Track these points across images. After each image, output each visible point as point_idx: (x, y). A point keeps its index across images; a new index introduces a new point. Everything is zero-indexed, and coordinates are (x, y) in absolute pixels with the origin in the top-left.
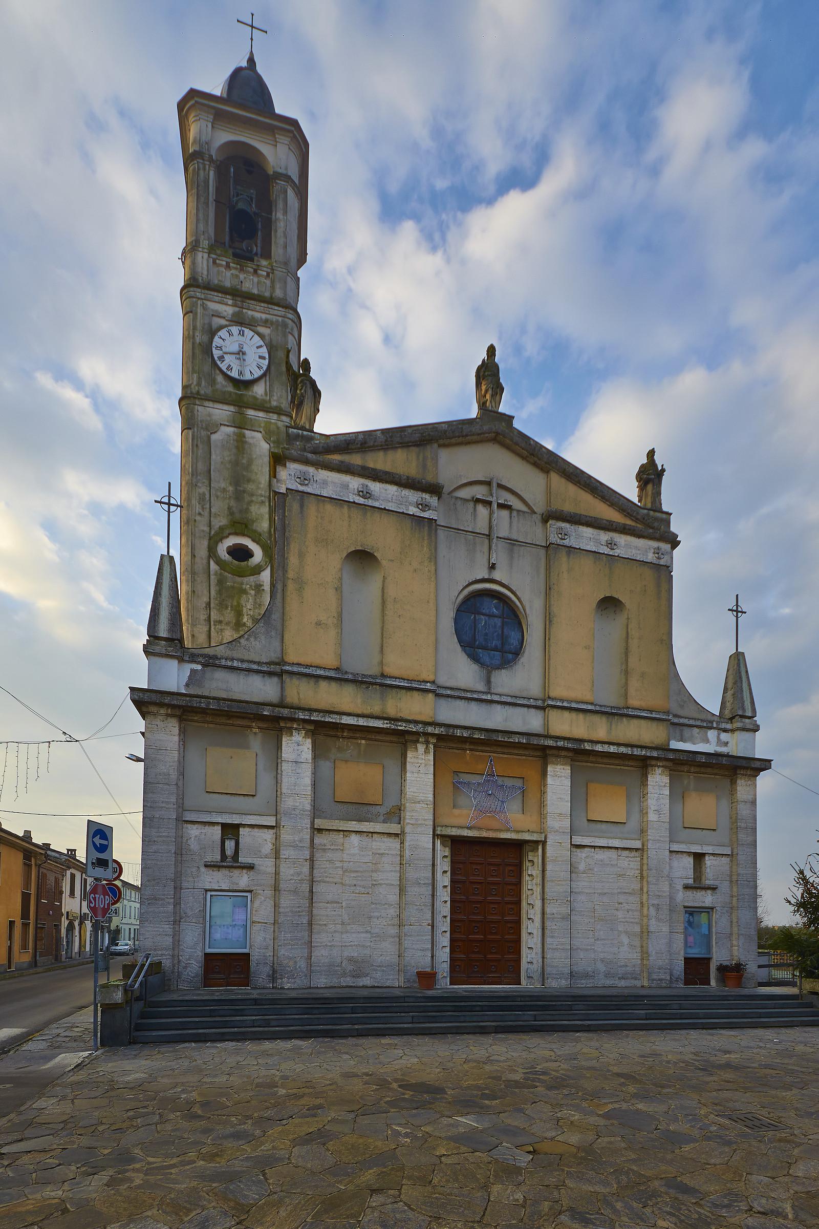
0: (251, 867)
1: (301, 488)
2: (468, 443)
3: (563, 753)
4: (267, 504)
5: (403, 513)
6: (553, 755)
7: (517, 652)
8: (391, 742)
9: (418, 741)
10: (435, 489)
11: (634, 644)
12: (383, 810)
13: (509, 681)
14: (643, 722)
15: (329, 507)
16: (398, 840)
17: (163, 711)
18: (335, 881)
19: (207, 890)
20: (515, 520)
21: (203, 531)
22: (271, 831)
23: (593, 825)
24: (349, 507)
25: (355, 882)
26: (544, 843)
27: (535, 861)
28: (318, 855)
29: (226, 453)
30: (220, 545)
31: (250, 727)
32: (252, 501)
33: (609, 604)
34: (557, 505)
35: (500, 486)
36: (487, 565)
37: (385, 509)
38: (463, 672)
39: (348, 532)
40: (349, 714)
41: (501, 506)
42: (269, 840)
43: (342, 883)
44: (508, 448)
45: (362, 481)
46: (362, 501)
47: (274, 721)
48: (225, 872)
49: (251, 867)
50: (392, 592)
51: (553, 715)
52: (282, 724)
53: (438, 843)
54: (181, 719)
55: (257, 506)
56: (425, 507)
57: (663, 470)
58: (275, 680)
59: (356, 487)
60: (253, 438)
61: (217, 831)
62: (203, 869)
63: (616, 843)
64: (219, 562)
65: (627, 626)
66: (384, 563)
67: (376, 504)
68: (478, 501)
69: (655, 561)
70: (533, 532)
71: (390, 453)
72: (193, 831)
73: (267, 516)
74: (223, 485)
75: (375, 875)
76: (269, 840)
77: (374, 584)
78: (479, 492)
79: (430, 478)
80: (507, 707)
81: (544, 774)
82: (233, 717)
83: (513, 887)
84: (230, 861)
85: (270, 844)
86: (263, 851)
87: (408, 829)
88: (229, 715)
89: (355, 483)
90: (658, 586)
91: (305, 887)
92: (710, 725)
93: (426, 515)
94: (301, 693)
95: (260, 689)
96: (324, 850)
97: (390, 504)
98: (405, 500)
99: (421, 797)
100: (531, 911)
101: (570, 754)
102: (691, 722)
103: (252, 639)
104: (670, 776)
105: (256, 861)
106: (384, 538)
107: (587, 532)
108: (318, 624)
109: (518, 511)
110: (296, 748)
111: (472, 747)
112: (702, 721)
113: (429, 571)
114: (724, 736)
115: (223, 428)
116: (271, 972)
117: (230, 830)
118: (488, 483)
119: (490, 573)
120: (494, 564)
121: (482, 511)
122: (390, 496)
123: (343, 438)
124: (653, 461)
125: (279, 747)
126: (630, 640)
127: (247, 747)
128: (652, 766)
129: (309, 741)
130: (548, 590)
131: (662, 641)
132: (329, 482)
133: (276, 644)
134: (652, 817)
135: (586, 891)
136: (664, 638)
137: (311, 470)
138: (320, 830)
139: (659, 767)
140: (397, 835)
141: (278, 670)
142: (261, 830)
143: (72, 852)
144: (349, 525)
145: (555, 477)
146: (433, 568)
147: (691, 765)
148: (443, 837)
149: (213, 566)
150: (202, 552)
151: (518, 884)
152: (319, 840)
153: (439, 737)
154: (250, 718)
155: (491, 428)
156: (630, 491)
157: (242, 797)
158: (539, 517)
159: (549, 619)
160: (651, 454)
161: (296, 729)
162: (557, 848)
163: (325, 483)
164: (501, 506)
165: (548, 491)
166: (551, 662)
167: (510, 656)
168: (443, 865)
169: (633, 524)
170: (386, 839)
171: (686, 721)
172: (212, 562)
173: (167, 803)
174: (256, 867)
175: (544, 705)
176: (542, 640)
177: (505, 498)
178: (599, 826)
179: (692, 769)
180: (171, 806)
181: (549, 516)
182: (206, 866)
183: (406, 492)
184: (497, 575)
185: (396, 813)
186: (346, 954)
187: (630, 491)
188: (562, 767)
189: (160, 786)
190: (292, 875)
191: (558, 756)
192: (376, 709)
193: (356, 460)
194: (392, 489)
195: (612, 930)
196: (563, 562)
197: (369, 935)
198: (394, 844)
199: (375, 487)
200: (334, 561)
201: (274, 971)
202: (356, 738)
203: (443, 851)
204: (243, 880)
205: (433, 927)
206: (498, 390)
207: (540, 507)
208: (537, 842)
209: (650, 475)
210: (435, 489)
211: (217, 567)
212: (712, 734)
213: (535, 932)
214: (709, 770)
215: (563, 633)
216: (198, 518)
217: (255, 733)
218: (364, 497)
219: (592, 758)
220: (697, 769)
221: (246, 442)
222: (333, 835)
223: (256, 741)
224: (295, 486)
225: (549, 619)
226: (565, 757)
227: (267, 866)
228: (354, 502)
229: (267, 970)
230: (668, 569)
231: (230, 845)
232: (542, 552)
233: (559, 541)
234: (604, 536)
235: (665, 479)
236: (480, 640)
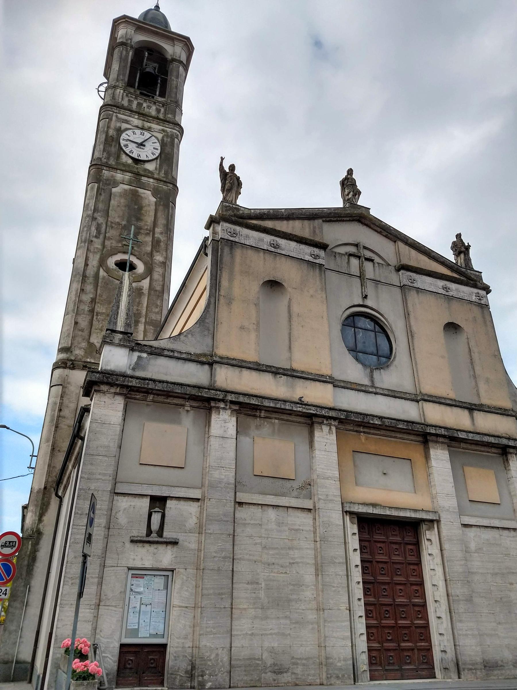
0: (175, 543)
1: (232, 239)
2: (343, 221)
3: (441, 440)
4: (151, 235)
5: (301, 259)
6: (433, 441)
7: (389, 355)
8: (299, 423)
9: (322, 423)
10: (323, 247)
11: (476, 356)
12: (295, 485)
13: (387, 379)
15: (250, 252)
16: (310, 516)
17: (113, 390)
18: (255, 558)
19: (129, 569)
20: (377, 269)
21: (97, 248)
22: (196, 504)
23: (475, 505)
24: (264, 253)
25: (273, 561)
26: (438, 521)
27: (433, 539)
28: (238, 530)
29: (122, 200)
30: (110, 259)
31: (183, 406)
32: (140, 232)
33: (452, 327)
34: (405, 261)
35: (365, 248)
36: (361, 295)
37: (289, 256)
38: (354, 371)
39: (265, 267)
41: (367, 259)
42: (194, 514)
43: (261, 561)
44: (367, 225)
45: (273, 238)
46: (273, 249)
47: (204, 401)
48: (152, 548)
49: (175, 543)
50: (295, 309)
51: (477, 415)
52: (213, 404)
53: (347, 518)
54: (126, 397)
55: (143, 236)
56: (317, 257)
57: (469, 246)
58: (207, 367)
59: (269, 241)
60: (144, 193)
61: (146, 502)
62: (128, 545)
64: (107, 270)
65: (468, 344)
66: (290, 289)
67: (283, 252)
68: (351, 255)
69: (477, 301)
70: (394, 278)
71: (291, 222)
72: (123, 503)
73: (150, 243)
74: (117, 220)
75: (291, 552)
76: (194, 514)
77: (282, 304)
78: (352, 250)
79: (317, 239)
81: (427, 457)
82: (171, 396)
83: (415, 567)
84: (154, 536)
85: (194, 518)
86: (187, 525)
87: (320, 505)
88: (168, 394)
89: (268, 238)
90: (484, 317)
91: (228, 565)
93: (317, 261)
94: (226, 378)
95: (193, 375)
96: (245, 525)
97: (292, 253)
98: (302, 251)
99: (329, 473)
100: (437, 594)
101: (446, 441)
103: (190, 336)
104: (449, 451)
105: (181, 537)
106: (288, 273)
107: (429, 280)
108: (242, 328)
109: (378, 263)
110: (223, 425)
111: (366, 430)
113: (322, 297)
115: (121, 185)
116: (189, 668)
117: (158, 502)
118: (357, 245)
119: (363, 302)
120: (366, 296)
121: (355, 262)
122: (292, 248)
123: (258, 211)
124: (462, 240)
125: (208, 423)
126: (472, 354)
127: (177, 421)
128: (511, 453)
129: (234, 419)
130: (407, 315)
131: (495, 356)
132: (252, 237)
133: (209, 341)
135: (480, 571)
136: (496, 354)
137: (238, 228)
138: (240, 504)
140: (309, 510)
141: (210, 361)
142: (486, 529)
144: (264, 264)
145: (401, 245)
146: (324, 296)
148: (351, 513)
149: (102, 273)
150: (94, 261)
151: (419, 563)
152: (242, 513)
153: (341, 421)
154: (185, 398)
155: (354, 214)
156: (450, 256)
158: (393, 268)
159: (410, 334)
160: (459, 236)
161: (224, 408)
162: (450, 526)
163: (247, 236)
164: (367, 259)
165: (398, 254)
166: (419, 366)
167: (384, 360)
168: (354, 543)
169: (458, 277)
170: (299, 513)
172: (101, 270)
173: (105, 475)
174: (180, 542)
175: (418, 398)
176: (409, 350)
177: (368, 254)
180: (107, 478)
181: (403, 268)
182: (132, 541)
183: (303, 246)
184: (369, 303)
185: (307, 487)
186: (266, 644)
187: (450, 256)
188: (441, 451)
189: (100, 458)
190: (215, 552)
191: (437, 442)
193: (269, 224)
194: (293, 244)
195: (509, 612)
196: (412, 297)
197: (288, 622)
198: (303, 520)
199: (282, 242)
200: (255, 287)
201: (193, 667)
202: (270, 418)
203: (353, 528)
204: (166, 557)
205: (350, 611)
206: (357, 193)
207: (393, 261)
208: (432, 521)
209: (461, 248)
210: (323, 247)
211: (105, 274)
213: (443, 616)
215: (422, 345)
216: (94, 239)
217: (188, 411)
218: (275, 247)
219: (462, 445)
221: (139, 196)
222: (253, 509)
223: (300, 434)
224: (227, 237)
225: (410, 334)
226: (442, 443)
227: (189, 541)
228: (268, 250)
229: (184, 665)
230: (487, 306)
231: (156, 518)
232: (398, 290)
233: (410, 284)
234: (441, 283)
235: (471, 251)
236: (360, 346)
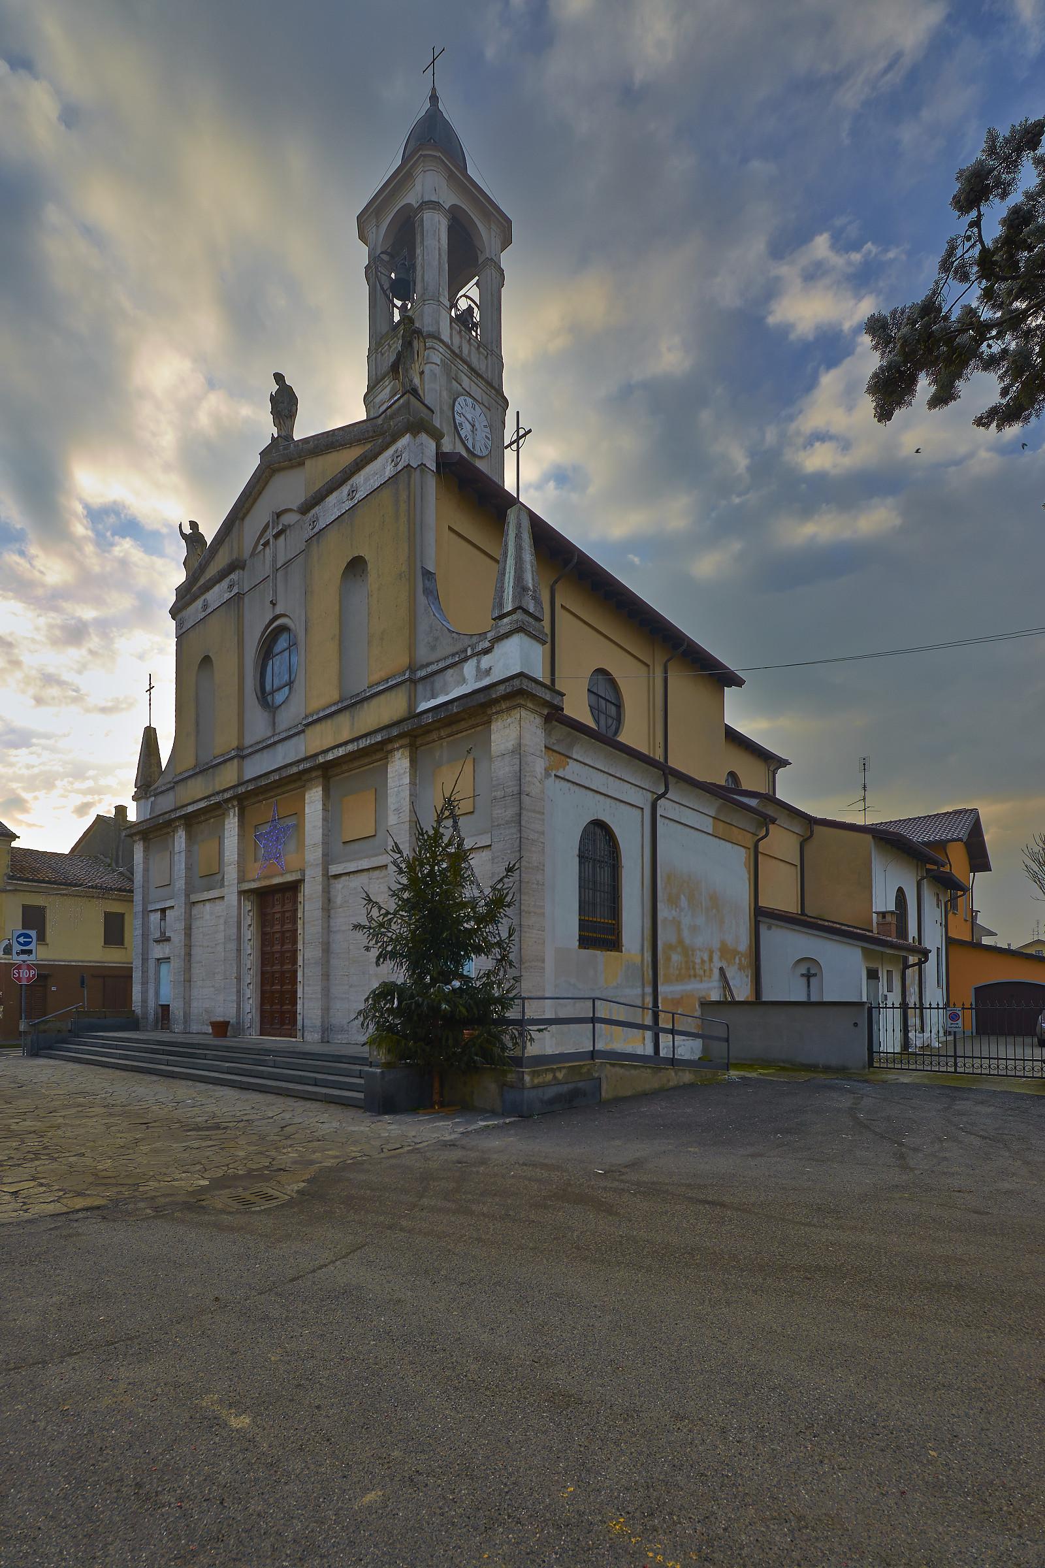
14: (382, 698)
40: (189, 804)
63: (365, 864)
80: (285, 743)
92: (463, 656)
102: (441, 665)
112: (453, 655)
114: (486, 661)
120: (206, 660)
134: (392, 819)
139: (398, 749)
143: (769, 928)
147: (438, 729)
157: (628, 807)
171: (434, 668)
178: (356, 846)
179: (443, 733)
192: (346, 736)
212: (469, 668)
214: (463, 725)
220: (448, 730)
